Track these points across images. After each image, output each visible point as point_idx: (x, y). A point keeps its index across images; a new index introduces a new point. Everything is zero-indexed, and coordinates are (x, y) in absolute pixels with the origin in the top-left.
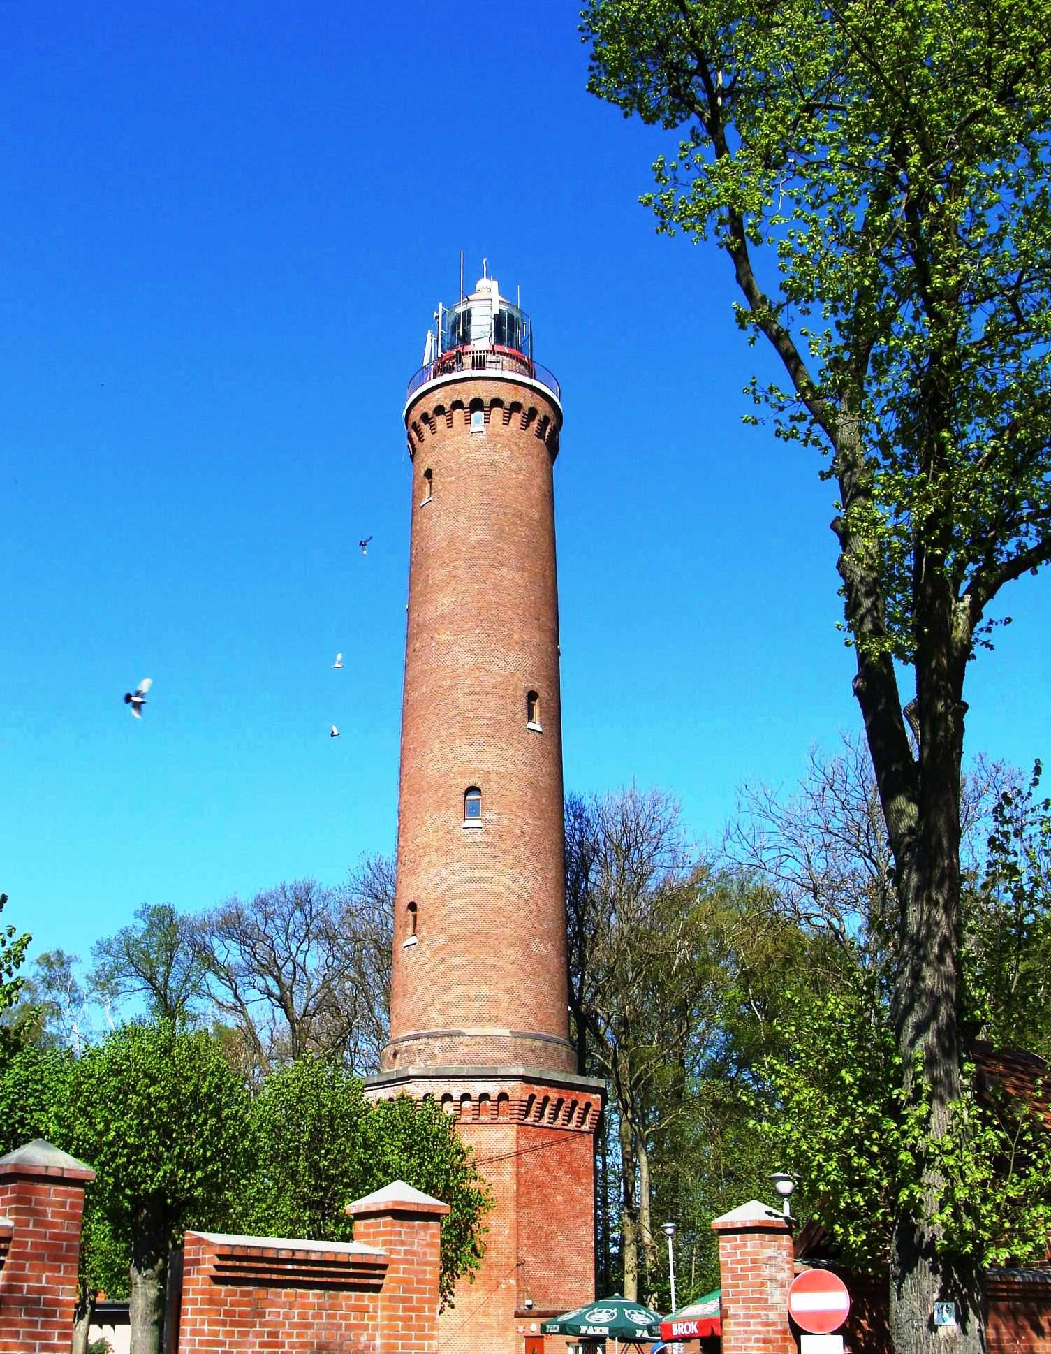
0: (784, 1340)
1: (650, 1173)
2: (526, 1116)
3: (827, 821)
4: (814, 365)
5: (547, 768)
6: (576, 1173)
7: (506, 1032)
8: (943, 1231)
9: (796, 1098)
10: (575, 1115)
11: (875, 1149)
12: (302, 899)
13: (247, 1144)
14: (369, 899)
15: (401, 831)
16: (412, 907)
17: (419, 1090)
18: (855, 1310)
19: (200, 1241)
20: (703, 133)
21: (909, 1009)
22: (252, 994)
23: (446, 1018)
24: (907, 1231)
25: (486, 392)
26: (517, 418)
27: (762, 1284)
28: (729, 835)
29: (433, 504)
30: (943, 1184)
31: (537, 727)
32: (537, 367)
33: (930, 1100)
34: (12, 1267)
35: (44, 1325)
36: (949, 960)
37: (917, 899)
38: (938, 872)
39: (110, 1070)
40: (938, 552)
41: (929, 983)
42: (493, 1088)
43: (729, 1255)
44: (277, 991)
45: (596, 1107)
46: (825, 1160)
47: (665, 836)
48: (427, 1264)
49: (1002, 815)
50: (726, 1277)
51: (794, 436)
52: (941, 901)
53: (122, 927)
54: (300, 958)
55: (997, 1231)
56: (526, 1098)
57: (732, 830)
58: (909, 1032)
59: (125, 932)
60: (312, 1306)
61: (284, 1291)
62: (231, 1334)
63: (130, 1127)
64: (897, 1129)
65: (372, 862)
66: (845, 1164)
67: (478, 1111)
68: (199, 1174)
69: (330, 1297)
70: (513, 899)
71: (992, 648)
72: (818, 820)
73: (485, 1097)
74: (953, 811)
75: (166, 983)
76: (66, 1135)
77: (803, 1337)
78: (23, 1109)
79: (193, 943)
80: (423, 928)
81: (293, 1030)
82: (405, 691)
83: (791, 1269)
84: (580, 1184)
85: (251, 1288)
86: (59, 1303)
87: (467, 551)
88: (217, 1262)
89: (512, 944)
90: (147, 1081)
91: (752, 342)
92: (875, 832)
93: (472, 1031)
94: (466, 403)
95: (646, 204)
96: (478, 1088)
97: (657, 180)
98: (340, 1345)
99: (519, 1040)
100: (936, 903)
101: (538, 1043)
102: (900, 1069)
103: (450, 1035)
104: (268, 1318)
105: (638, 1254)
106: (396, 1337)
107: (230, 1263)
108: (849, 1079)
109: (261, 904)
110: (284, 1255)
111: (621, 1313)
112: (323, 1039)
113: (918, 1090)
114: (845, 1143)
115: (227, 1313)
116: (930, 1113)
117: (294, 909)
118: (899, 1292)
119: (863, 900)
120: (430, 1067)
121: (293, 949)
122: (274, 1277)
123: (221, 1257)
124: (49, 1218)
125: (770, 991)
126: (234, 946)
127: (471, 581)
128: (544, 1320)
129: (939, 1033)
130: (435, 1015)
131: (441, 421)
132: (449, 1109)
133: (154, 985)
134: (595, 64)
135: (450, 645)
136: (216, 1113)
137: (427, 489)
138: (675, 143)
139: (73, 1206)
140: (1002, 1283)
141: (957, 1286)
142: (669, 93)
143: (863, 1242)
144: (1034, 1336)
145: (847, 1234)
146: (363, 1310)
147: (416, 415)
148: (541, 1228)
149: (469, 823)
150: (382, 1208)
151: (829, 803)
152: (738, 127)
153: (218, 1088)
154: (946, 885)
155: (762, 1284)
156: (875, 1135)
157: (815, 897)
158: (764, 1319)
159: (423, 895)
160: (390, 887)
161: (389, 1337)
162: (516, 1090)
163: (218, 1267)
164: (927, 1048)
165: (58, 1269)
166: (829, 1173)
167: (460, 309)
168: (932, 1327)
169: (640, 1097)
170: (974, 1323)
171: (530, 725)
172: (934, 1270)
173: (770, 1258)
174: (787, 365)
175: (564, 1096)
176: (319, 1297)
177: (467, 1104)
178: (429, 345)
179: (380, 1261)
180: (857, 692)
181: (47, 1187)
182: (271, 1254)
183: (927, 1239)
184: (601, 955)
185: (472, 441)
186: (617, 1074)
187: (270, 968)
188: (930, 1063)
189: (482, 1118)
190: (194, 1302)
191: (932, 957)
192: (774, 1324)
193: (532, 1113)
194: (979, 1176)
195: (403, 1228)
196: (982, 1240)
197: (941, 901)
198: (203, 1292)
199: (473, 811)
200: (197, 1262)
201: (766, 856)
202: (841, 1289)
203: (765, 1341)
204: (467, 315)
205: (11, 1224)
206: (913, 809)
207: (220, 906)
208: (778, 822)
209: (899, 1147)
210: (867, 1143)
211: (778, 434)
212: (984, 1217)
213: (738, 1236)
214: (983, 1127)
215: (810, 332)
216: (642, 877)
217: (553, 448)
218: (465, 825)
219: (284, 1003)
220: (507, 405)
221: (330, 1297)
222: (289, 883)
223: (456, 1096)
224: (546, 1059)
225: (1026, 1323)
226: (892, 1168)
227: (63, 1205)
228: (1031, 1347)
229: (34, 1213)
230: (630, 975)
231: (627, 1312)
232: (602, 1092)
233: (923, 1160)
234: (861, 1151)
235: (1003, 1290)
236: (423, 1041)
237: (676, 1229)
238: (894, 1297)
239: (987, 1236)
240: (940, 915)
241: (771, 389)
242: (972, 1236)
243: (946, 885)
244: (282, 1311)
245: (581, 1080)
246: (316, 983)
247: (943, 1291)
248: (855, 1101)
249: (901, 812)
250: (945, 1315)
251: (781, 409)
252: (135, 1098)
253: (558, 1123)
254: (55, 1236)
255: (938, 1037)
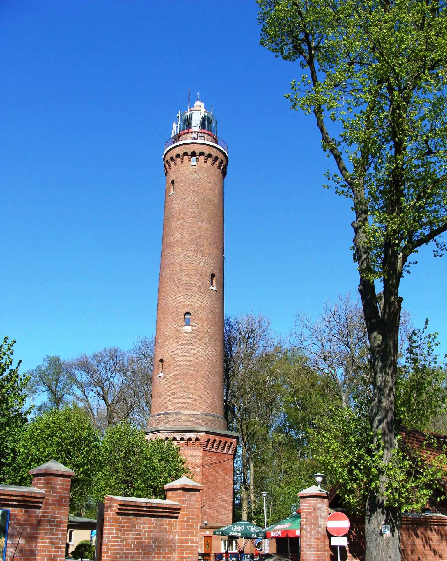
0: (325, 538)
1: (255, 471)
2: (206, 447)
3: (331, 330)
4: (348, 163)
5: (218, 306)
6: (225, 470)
7: (199, 413)
8: (387, 498)
9: (333, 447)
10: (226, 447)
11: (362, 467)
12: (113, 355)
13: (101, 458)
14: (141, 356)
15: (157, 329)
16: (417, 262)
17: (163, 436)
18: (351, 527)
19: (111, 499)
20: (305, 63)
21: (376, 414)
22: (92, 394)
23: (174, 407)
24: (373, 498)
25: (198, 149)
26: (210, 160)
27: (317, 517)
28: (291, 335)
29: (174, 195)
30: (387, 481)
31: (214, 288)
32: (218, 139)
33: (383, 449)
34: (45, 508)
35: (56, 530)
36: (392, 396)
37: (380, 372)
38: (389, 362)
39: (45, 427)
40: (397, 242)
41: (384, 404)
42: (193, 436)
43: (304, 506)
44: (101, 393)
45: (234, 444)
46: (342, 471)
47: (264, 334)
48: (196, 508)
49: (412, 339)
50: (303, 514)
51: (342, 194)
52: (390, 373)
53: (38, 365)
54: (111, 380)
55: (407, 498)
56: (207, 440)
57: (293, 333)
58: (376, 423)
59: (39, 367)
60: (153, 524)
61: (143, 518)
62: (123, 534)
63: (54, 450)
64: (371, 460)
65: (143, 341)
66: (350, 472)
67: (187, 445)
68: (81, 470)
69: (159, 520)
70: (203, 359)
71: (409, 273)
72: (327, 330)
73: (190, 439)
74: (396, 339)
75: (56, 389)
76: (27, 453)
77: (332, 538)
78: (7, 441)
79: (67, 373)
80: (166, 370)
81: (108, 409)
82: (161, 272)
83: (328, 512)
84: (227, 475)
85: (131, 517)
86: (61, 522)
87: (188, 215)
88: (119, 507)
89: (202, 377)
90: (61, 432)
91: (328, 156)
92: (350, 335)
93: (185, 412)
94: (189, 153)
95: (287, 98)
96: (187, 435)
97: (292, 89)
98: (163, 539)
99: (204, 416)
100: (388, 374)
101: (212, 418)
102: (372, 437)
103: (176, 414)
104: (137, 528)
105: (249, 504)
106: (184, 536)
107: (123, 507)
108: (353, 440)
109: (96, 356)
110: (143, 505)
111: (246, 528)
112: (119, 414)
113: (379, 445)
114: (350, 464)
115: (122, 526)
116: (383, 454)
117: (110, 359)
118: (369, 521)
119: (344, 363)
120: (168, 426)
121: (109, 376)
122: (140, 513)
123: (120, 505)
124: (58, 490)
125: (303, 398)
126: (84, 374)
127: (189, 227)
128: (215, 530)
129: (388, 423)
130: (170, 405)
131: (178, 160)
132: (175, 443)
133: (51, 389)
134: (263, 33)
135: (180, 253)
136: (88, 445)
137: (172, 188)
138: (296, 71)
139: (67, 485)
140: (404, 518)
141: (391, 519)
142: (293, 47)
143: (356, 502)
144: (415, 537)
145: (349, 499)
146: (171, 525)
147: (168, 158)
148: (211, 493)
149: (186, 327)
150: (179, 487)
151: (332, 323)
152: (318, 61)
153: (89, 435)
154: (392, 367)
155: (317, 517)
156: (362, 462)
157: (325, 361)
158: (317, 531)
159: (166, 356)
160: (150, 351)
161: (181, 536)
162: (202, 436)
163: (119, 509)
164: (383, 429)
165: (61, 509)
166: (344, 476)
167: (188, 114)
168: (381, 534)
169: (251, 439)
170: (397, 533)
171: (212, 288)
172: (383, 513)
173: (320, 508)
174: (336, 160)
175: (222, 439)
176: (155, 520)
177: (183, 442)
178: (174, 128)
179: (178, 507)
180: (360, 291)
181: (57, 478)
182: (139, 504)
183: (380, 501)
184: (235, 382)
185: (191, 169)
186: (242, 431)
187: (99, 383)
188: (384, 434)
189: (188, 448)
190: (109, 522)
191: (386, 395)
192: (321, 532)
193: (209, 446)
194: (401, 478)
195: (187, 494)
196: (401, 502)
197: (390, 373)
198: (113, 518)
199: (187, 322)
200: (110, 507)
201: (306, 344)
202: (345, 520)
203: (317, 539)
204: (191, 116)
205: (44, 492)
206: (380, 337)
207: (79, 357)
208: (311, 330)
209: (371, 466)
210: (359, 465)
211: (336, 192)
212: (403, 493)
213: (308, 499)
214: (403, 459)
215: (349, 152)
216: (253, 351)
217: (224, 173)
218: (184, 328)
219: (105, 398)
220: (206, 155)
221: (159, 520)
222: (108, 348)
223: (178, 438)
224: (215, 425)
225: (413, 533)
226: (367, 475)
227: (63, 485)
228: (414, 542)
229: (52, 488)
230: (248, 390)
231: (248, 527)
232: (237, 438)
233: (381, 472)
234: (357, 467)
235: (404, 521)
236: (165, 416)
237: (267, 494)
238: (367, 523)
239: (403, 501)
240: (389, 378)
241: (335, 176)
242: (397, 501)
243: (392, 367)
244: (142, 526)
245: (230, 433)
246: (118, 389)
247: (386, 521)
248: (355, 449)
249: (375, 338)
250: (386, 530)
251: (338, 183)
252: (56, 438)
253: (219, 450)
254: (60, 497)
255: (387, 425)
